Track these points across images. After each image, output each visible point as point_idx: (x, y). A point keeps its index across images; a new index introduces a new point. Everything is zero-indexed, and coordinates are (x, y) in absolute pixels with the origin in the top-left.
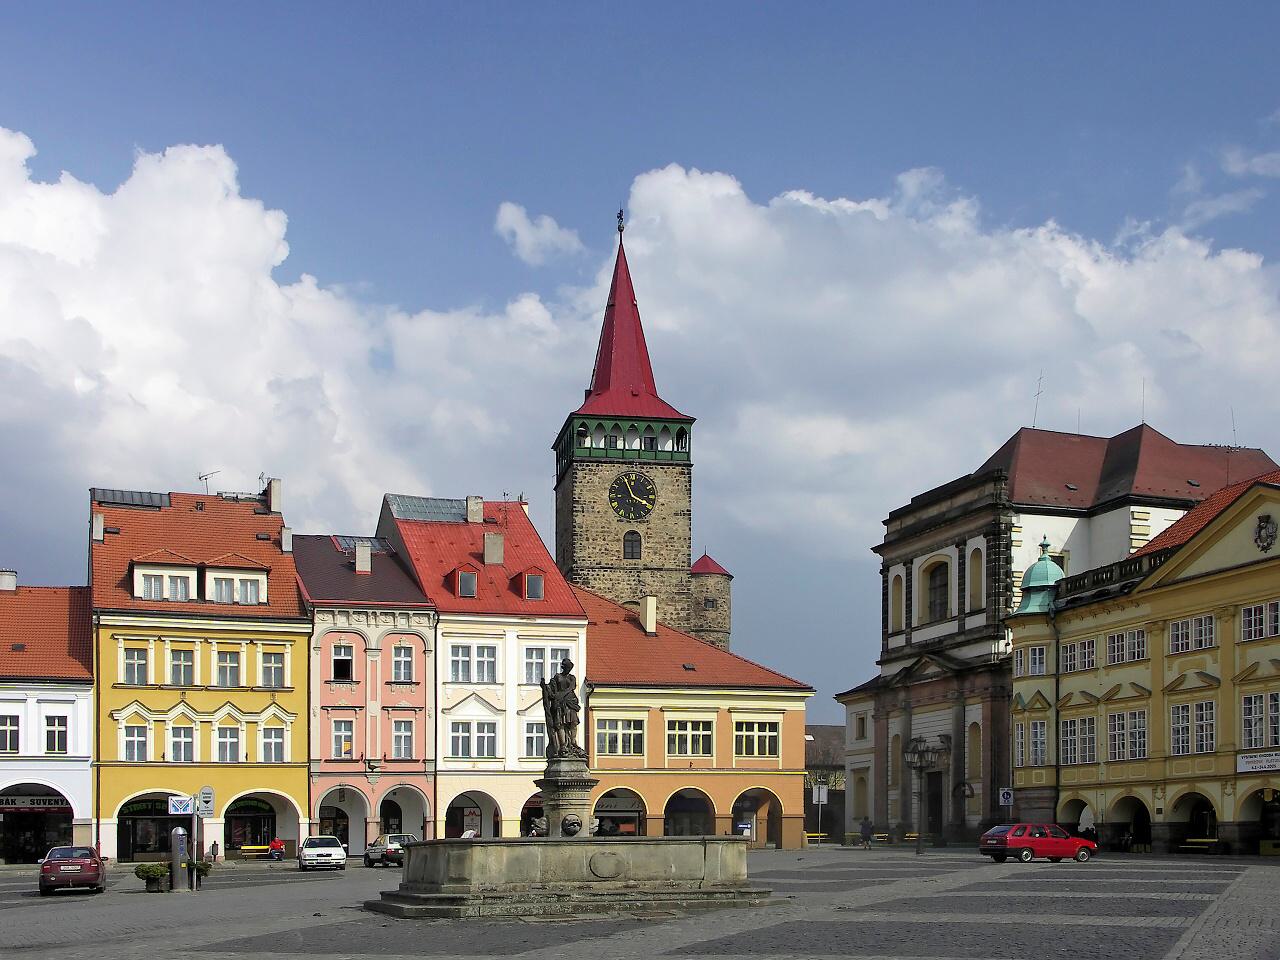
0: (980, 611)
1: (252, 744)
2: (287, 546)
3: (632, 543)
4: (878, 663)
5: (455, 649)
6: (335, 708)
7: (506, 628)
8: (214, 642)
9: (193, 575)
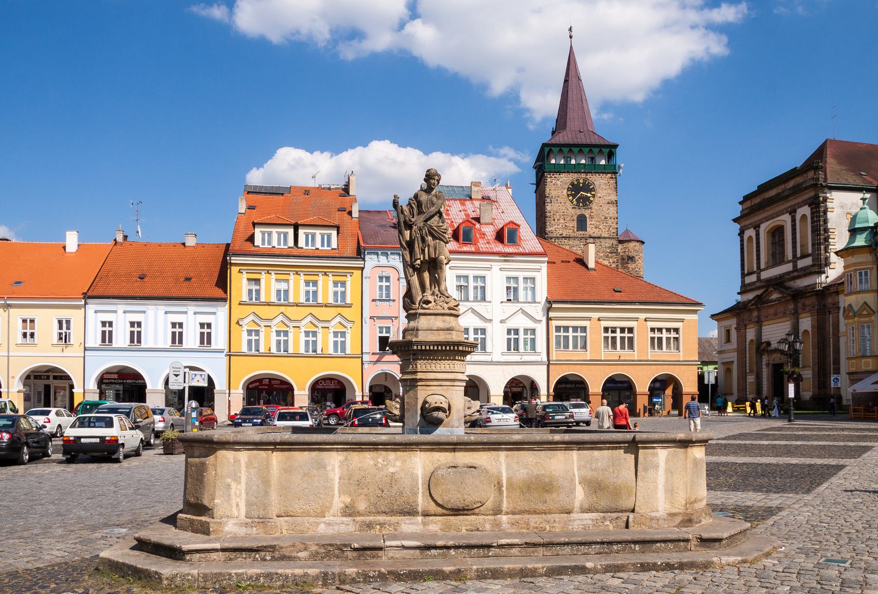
0: (807, 256)
1: (326, 342)
2: (355, 214)
3: (582, 222)
4: (738, 293)
5: (459, 277)
6: (379, 318)
7: (492, 263)
8: (273, 273)
9: (291, 231)
